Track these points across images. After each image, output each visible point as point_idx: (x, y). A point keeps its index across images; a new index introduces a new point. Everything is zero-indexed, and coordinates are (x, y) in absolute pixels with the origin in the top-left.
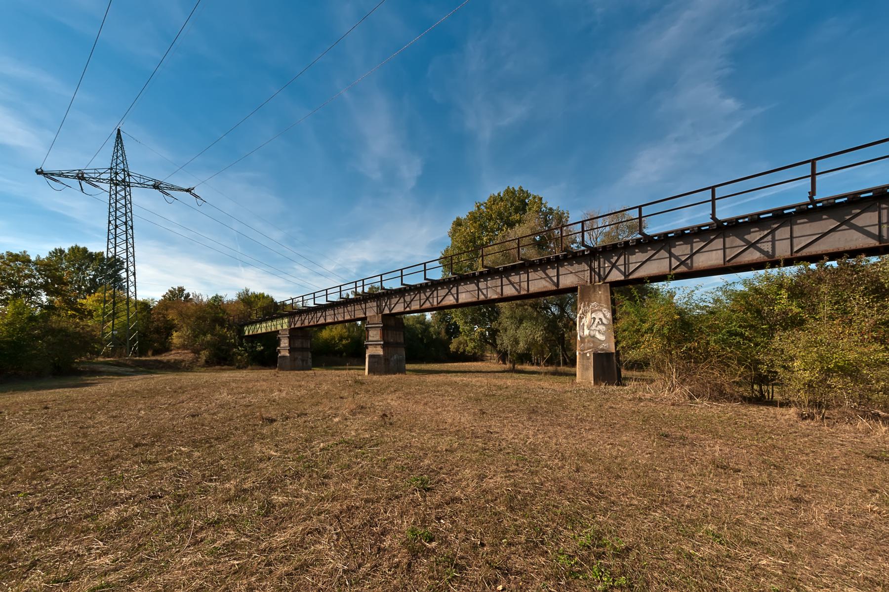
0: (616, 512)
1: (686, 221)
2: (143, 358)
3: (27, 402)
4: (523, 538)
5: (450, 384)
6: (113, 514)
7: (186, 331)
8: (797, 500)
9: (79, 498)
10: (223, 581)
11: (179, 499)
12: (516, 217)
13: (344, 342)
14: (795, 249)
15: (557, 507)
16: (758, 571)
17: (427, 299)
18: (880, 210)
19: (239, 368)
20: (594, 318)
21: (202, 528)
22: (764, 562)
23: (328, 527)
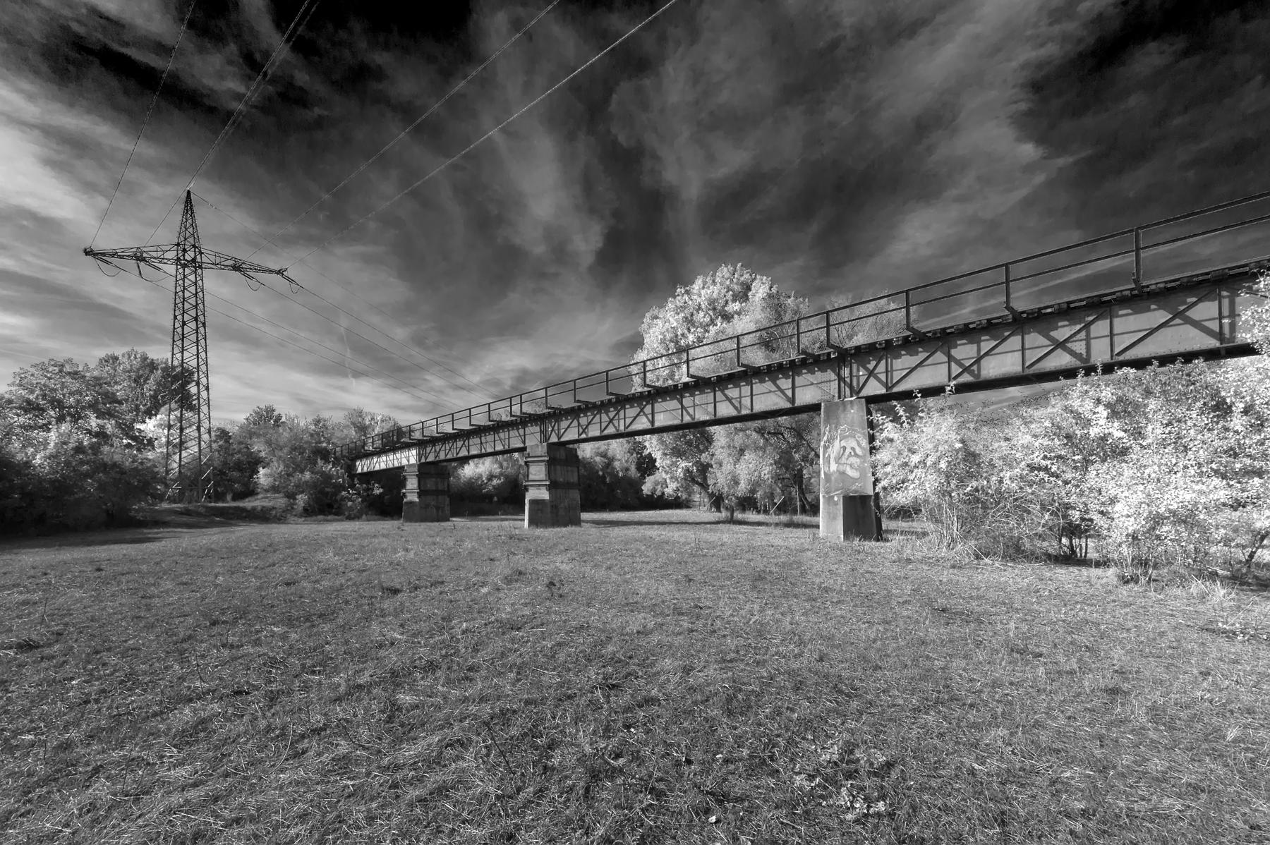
0: (873, 715)
1: (973, 312)
2: (220, 505)
3: (75, 561)
4: (745, 752)
5: (644, 540)
6: (186, 714)
7: (278, 467)
8: (1113, 691)
9: (145, 690)
10: (334, 806)
11: (272, 699)
12: (735, 306)
13: (495, 482)
14: (1117, 351)
15: (792, 710)
16: (1059, 786)
17: (611, 421)
18: (1220, 298)
19: (350, 518)
20: (845, 448)
21: (303, 737)
22: (1068, 774)
23: (474, 737)
